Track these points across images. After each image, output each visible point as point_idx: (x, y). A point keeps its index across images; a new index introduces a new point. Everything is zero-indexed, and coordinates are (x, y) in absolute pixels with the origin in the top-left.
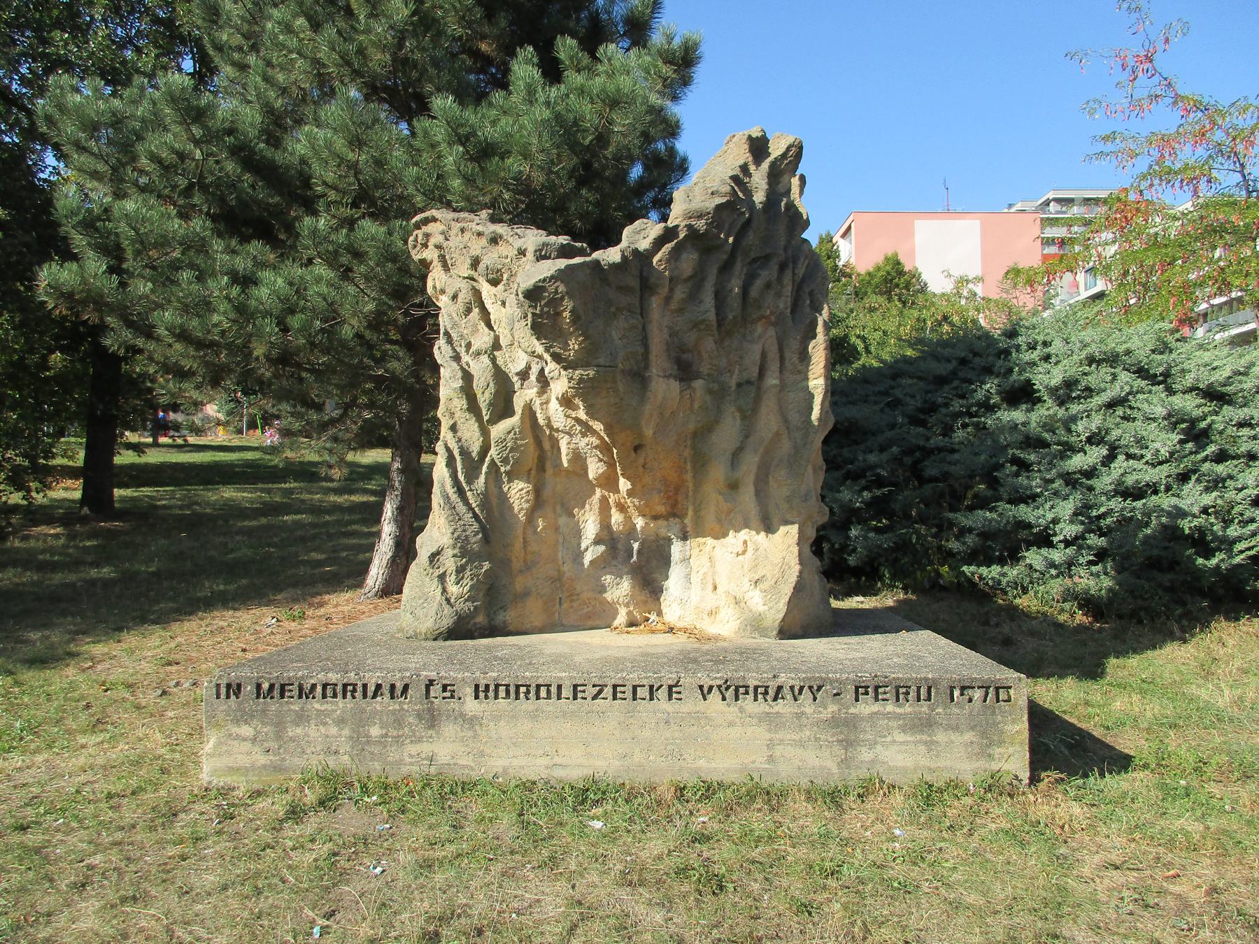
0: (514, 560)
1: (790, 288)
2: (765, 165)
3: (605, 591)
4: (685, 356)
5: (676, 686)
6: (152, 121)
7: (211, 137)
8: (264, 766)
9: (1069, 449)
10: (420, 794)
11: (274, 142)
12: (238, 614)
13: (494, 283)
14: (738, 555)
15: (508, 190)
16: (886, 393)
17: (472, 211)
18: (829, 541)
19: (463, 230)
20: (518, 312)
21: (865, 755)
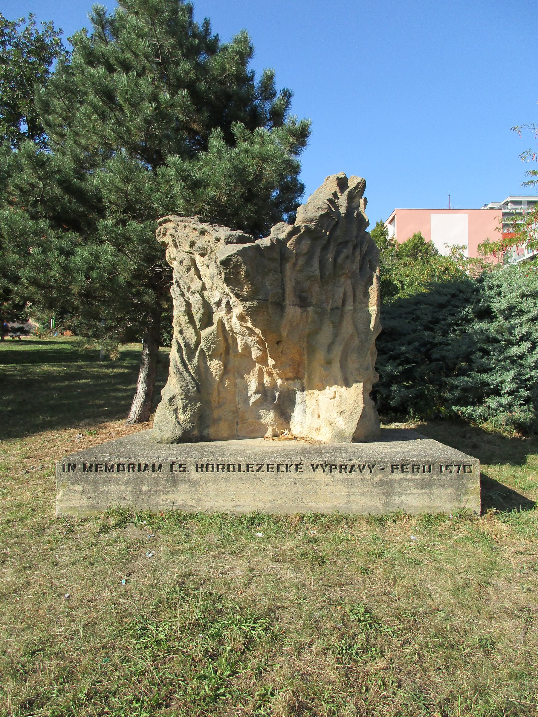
0: (213, 402)
2: (346, 193)
3: (261, 418)
4: (303, 294)
5: (299, 465)
6: (15, 166)
7: (49, 175)
8: (88, 506)
9: (511, 344)
10: (168, 520)
11: (81, 177)
12: (60, 432)
13: (203, 255)
14: (331, 399)
15: (208, 205)
16: (411, 313)
17: (189, 216)
18: (380, 393)
19: (185, 227)
20: (216, 271)
21: (397, 500)
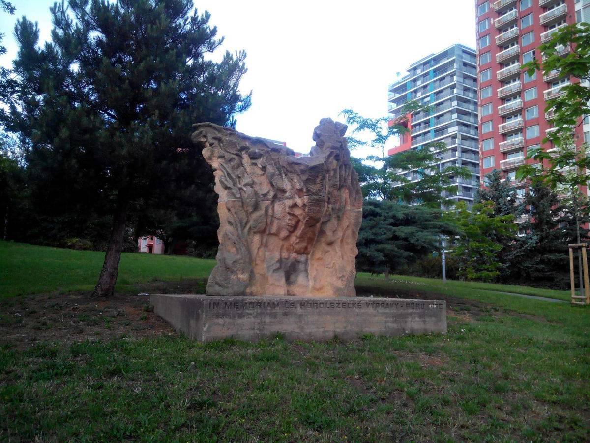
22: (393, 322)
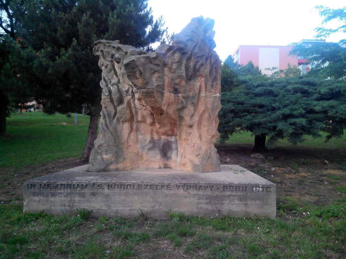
1: (209, 66)
14: (192, 147)
22: (207, 203)
